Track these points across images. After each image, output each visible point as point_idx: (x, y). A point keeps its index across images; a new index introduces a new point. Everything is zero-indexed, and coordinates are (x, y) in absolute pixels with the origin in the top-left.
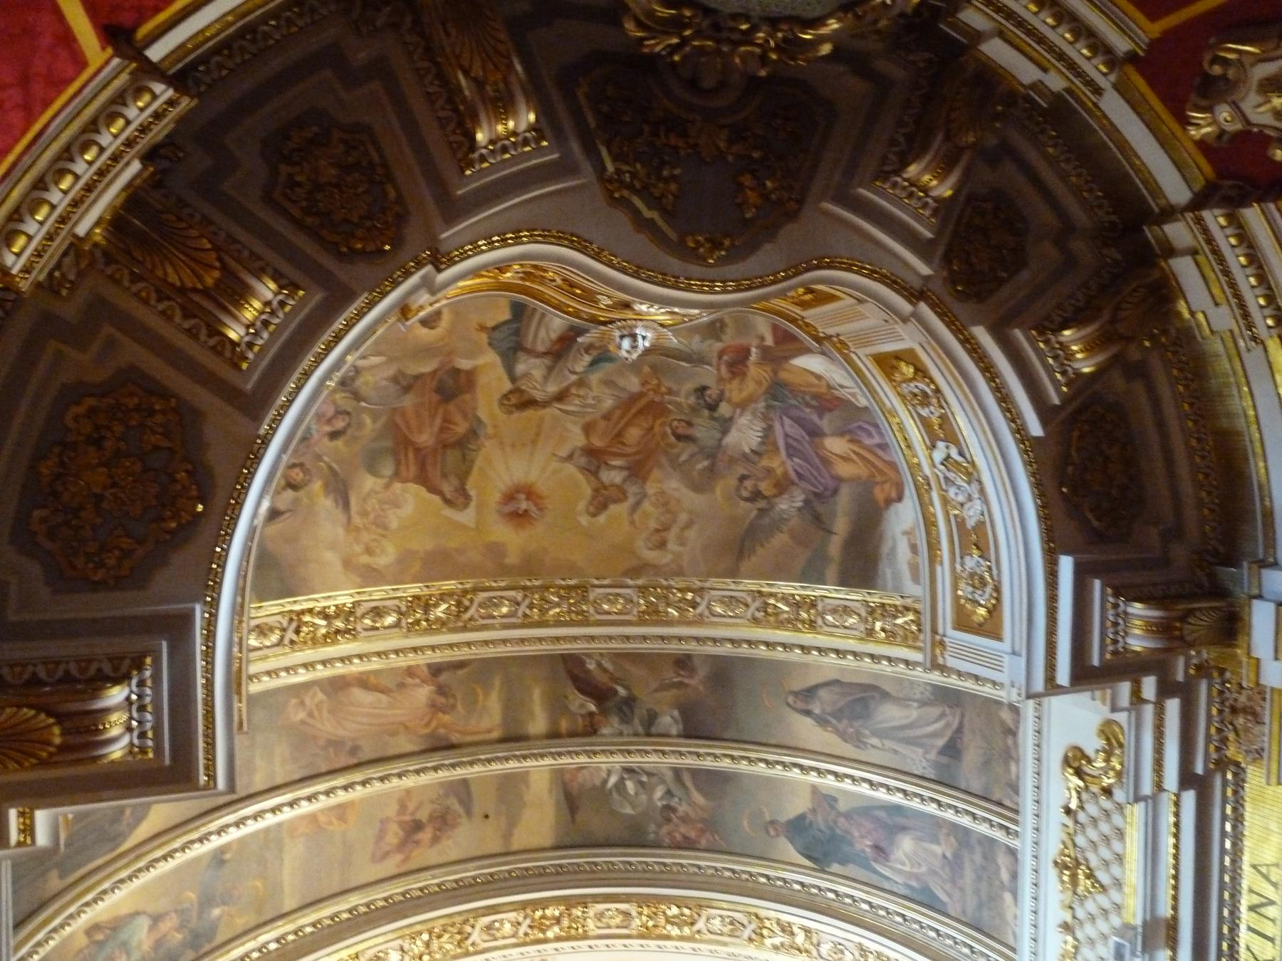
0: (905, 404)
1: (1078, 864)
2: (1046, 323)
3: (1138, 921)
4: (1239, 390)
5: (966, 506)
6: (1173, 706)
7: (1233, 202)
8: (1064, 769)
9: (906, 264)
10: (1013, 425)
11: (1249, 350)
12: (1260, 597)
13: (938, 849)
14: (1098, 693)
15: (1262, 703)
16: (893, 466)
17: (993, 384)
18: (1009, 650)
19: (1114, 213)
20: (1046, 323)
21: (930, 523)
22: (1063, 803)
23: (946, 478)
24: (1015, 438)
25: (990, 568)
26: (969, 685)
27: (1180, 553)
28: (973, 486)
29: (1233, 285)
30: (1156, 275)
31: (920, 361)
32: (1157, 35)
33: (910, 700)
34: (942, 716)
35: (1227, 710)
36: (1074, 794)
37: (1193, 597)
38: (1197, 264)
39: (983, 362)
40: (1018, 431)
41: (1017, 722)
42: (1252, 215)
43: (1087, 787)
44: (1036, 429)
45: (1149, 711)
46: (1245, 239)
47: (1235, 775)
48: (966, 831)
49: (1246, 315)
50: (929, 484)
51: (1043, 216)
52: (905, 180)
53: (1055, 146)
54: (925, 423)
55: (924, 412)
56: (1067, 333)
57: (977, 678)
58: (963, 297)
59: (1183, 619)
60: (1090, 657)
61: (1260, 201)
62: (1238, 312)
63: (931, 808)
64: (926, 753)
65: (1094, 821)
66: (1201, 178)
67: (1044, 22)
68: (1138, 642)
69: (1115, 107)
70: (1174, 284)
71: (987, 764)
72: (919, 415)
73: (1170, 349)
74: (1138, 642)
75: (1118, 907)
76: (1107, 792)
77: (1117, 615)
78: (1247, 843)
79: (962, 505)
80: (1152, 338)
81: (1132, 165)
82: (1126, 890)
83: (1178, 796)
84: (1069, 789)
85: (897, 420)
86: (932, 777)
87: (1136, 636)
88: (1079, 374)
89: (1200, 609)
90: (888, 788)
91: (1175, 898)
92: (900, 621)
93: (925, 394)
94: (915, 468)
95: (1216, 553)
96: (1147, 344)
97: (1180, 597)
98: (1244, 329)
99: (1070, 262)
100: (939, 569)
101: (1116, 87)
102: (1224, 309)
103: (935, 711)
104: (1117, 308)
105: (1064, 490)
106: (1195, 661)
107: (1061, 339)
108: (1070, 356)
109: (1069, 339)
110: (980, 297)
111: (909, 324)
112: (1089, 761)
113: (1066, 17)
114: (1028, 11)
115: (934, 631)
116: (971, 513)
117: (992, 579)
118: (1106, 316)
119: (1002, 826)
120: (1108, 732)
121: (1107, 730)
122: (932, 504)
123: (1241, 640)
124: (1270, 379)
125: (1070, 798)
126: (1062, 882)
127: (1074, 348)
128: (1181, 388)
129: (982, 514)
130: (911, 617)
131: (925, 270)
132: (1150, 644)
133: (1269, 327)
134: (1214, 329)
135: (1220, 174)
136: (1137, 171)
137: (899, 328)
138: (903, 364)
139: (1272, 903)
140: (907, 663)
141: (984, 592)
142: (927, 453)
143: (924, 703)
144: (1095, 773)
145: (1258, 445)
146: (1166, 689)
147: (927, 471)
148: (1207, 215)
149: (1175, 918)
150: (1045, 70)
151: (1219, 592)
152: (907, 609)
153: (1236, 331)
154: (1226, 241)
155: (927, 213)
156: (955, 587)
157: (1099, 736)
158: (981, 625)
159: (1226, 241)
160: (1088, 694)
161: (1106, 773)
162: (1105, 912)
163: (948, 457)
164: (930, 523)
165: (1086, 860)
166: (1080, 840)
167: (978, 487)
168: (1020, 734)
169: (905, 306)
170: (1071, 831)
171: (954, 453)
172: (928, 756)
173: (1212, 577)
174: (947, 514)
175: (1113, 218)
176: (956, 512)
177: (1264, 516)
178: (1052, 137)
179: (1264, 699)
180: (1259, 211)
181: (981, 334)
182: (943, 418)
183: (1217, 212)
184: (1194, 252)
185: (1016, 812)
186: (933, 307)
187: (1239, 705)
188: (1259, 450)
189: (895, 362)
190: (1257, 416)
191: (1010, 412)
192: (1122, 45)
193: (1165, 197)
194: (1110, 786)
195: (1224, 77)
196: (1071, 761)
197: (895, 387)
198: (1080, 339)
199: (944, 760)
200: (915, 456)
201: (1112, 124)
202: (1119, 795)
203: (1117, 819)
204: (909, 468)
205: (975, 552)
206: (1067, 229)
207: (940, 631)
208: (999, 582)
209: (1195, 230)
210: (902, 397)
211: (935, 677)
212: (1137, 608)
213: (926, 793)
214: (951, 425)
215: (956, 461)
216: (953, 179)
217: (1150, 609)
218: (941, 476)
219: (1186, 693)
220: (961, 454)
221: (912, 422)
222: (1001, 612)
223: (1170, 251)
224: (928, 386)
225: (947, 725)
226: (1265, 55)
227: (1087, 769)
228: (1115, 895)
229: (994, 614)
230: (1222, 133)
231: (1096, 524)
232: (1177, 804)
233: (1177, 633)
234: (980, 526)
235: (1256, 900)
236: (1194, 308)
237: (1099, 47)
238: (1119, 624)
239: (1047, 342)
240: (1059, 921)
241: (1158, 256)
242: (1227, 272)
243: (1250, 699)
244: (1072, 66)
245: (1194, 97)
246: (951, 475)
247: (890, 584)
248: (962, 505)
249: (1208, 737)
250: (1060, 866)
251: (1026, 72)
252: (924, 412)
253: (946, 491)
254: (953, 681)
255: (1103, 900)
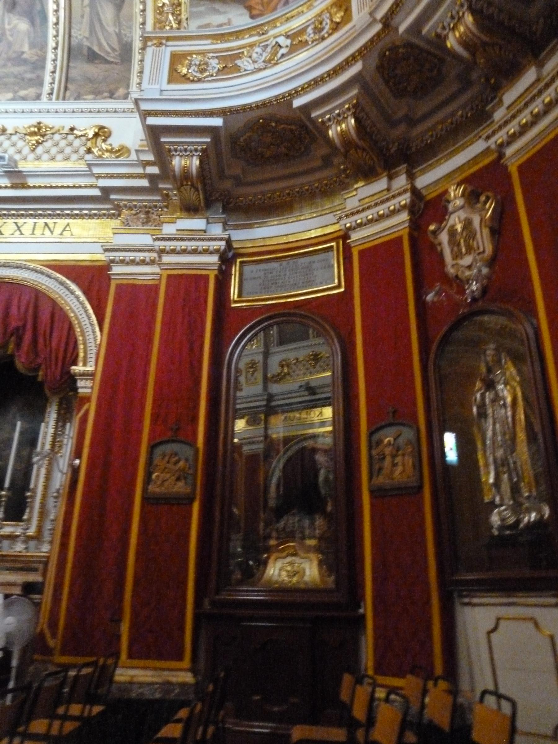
0: (315, 17)
1: (43, 136)
2: (360, 108)
3: (20, 169)
4: (314, 212)
5: (249, 60)
6: (145, 183)
7: (412, 208)
8: (96, 126)
9: (409, 14)
10: (300, 89)
11: (335, 215)
12: (208, 223)
13: (26, 48)
14: (145, 143)
15: (154, 225)
16: (275, 9)
17: (326, 76)
18: (163, 89)
19: (416, 149)
20: (360, 108)
21: (238, 34)
22: (76, 127)
23: (266, 46)
24: (292, 90)
25: (212, 76)
26: (136, 67)
27: (228, 184)
28: (263, 64)
29: (369, 208)
30: (379, 170)
31: (343, 26)
32: (509, 169)
33: (119, 26)
34: (114, 50)
35: (147, 210)
36: (83, 133)
37: (205, 193)
38: (382, 191)
39: (340, 69)
40: (296, 92)
41: (118, 98)
42: (404, 216)
43: (88, 140)
44: (297, 103)
45: (140, 170)
46: (393, 213)
47: (113, 215)
48: (43, 67)
49: (353, 214)
50: (263, 34)
51: (424, 107)
52: (463, 14)
53: (462, 116)
54: (302, 31)
55: (310, 30)
56: (353, 121)
57: (141, 72)
58: (382, 56)
59: (192, 185)
60: (165, 137)
61: (411, 220)
62: (355, 210)
63: (51, 43)
64: (87, 38)
65: (70, 144)
66: (427, 193)
67: (547, 97)
68: (177, 163)
69: (479, 147)
70: (373, 180)
71: (90, 80)
72: (308, 26)
73: (338, 179)
74: (177, 163)
75: (25, 159)
76: (89, 151)
77: (191, 151)
78: (80, 221)
79: (250, 57)
80: (345, 170)
81: (441, 159)
82: (36, 162)
83: (96, 187)
84: (85, 130)
85: (305, 11)
86: (72, 43)
87: (180, 162)
88: (328, 128)
89: (199, 194)
90: (57, 11)
91: (40, 187)
92: (171, 17)
93: (322, 29)
94: (273, 23)
95: (228, 203)
96: (342, 167)
97: (204, 185)
98: (345, 213)
99: (392, 124)
100: (209, 42)
101: (488, 149)
102: (357, 204)
103: (116, 46)
104: (364, 150)
105: (261, 121)
106: (170, 193)
107: (349, 118)
108: (339, 123)
109: (349, 121)
110: (380, 68)
111: (369, 16)
112: (104, 141)
113: (548, 108)
114: (547, 97)
115: (168, 39)
116: (246, 63)
117: (205, 78)
118: (361, 143)
119: (52, 89)
120: (122, 151)
121: (124, 150)
122: (251, 36)
123: (184, 214)
124: (320, 226)
125: (81, 131)
126: (29, 127)
127: (344, 126)
128: (316, 185)
129: (245, 70)
130: (175, 26)
131: (402, 29)
132: (177, 169)
133: (345, 225)
134: (347, 200)
135: (428, 203)
136: (437, 161)
137: (367, 10)
138: (342, 14)
139: (52, 232)
140: (143, 24)
141: (197, 72)
142: (283, 33)
143: (119, 35)
144: (98, 144)
145: (286, 221)
146: (152, 178)
147: (272, 33)
148: (408, 195)
149: (29, 187)
150: (508, 108)
151: (208, 204)
152: (179, 23)
153: (345, 210)
154: (392, 205)
155: (439, 30)
156: (198, 53)
157: (120, 146)
158: (176, 70)
159: (392, 205)
160: (144, 138)
161: (100, 150)
162: (20, 152)
163: (280, 47)
164: (238, 34)
165: (46, 141)
166: (57, 137)
167: (262, 67)
168: (110, 100)
169: (379, 15)
170: (61, 132)
171: (283, 51)
172: (85, 40)
173: (217, 200)
174: (244, 47)
175: (414, 149)
176: (246, 53)
177: (250, 224)
178: (467, 113)
179: (155, 226)
180: (405, 220)
181: (357, 68)
182: (306, 43)
183: (408, 200)
184: (388, 190)
185: (64, 99)
186: (378, 35)
187: (150, 215)
188: (283, 221)
189: (344, 7)
190: (300, 220)
191: (308, 87)
192: (509, 151)
193: (419, 176)
194: (93, 153)
195: (478, 201)
196: (102, 130)
197: (327, 9)
198: (349, 129)
199: (85, 52)
200: (282, 24)
201: (467, 147)
202: (89, 157)
203: (74, 157)
204: (273, 20)
205: (220, 66)
206: (412, 122)
207: (169, 43)
208: (204, 82)
209: (400, 190)
210: (320, 15)
211: (137, 44)
212: (196, 162)
213: (60, 38)
214: (302, 48)
215: (278, 52)
216: (459, 49)
217: (196, 169)
218: (268, 43)
219: (153, 189)
220: (283, 55)
221: (304, 21)
222: (186, 83)
223: (391, 178)
224: (327, 32)
225: (108, 53)
226: (484, 220)
227: (99, 140)
228: (31, 156)
229: (183, 78)
230: (449, 202)
231: (242, 139)
232: (91, 186)
233: (185, 183)
234: (237, 68)
235: (51, 226)
236: (359, 190)
237: (513, 138)
238: (186, 153)
239: (349, 109)
240: (6, 126)
241: (389, 171)
242: (376, 205)
243: (155, 219)
244: (506, 123)
245: (469, 189)
246: (269, 49)
247: (195, 10)
248: (250, 57)
249: (130, 201)
250: (39, 125)
251: (509, 97)
252: (310, 30)
253: (259, 46)
254: (137, 57)
255: (26, 150)
